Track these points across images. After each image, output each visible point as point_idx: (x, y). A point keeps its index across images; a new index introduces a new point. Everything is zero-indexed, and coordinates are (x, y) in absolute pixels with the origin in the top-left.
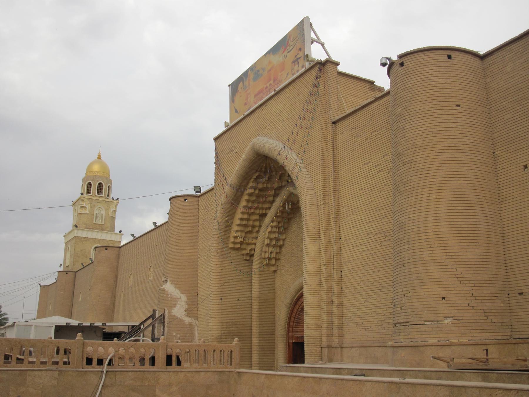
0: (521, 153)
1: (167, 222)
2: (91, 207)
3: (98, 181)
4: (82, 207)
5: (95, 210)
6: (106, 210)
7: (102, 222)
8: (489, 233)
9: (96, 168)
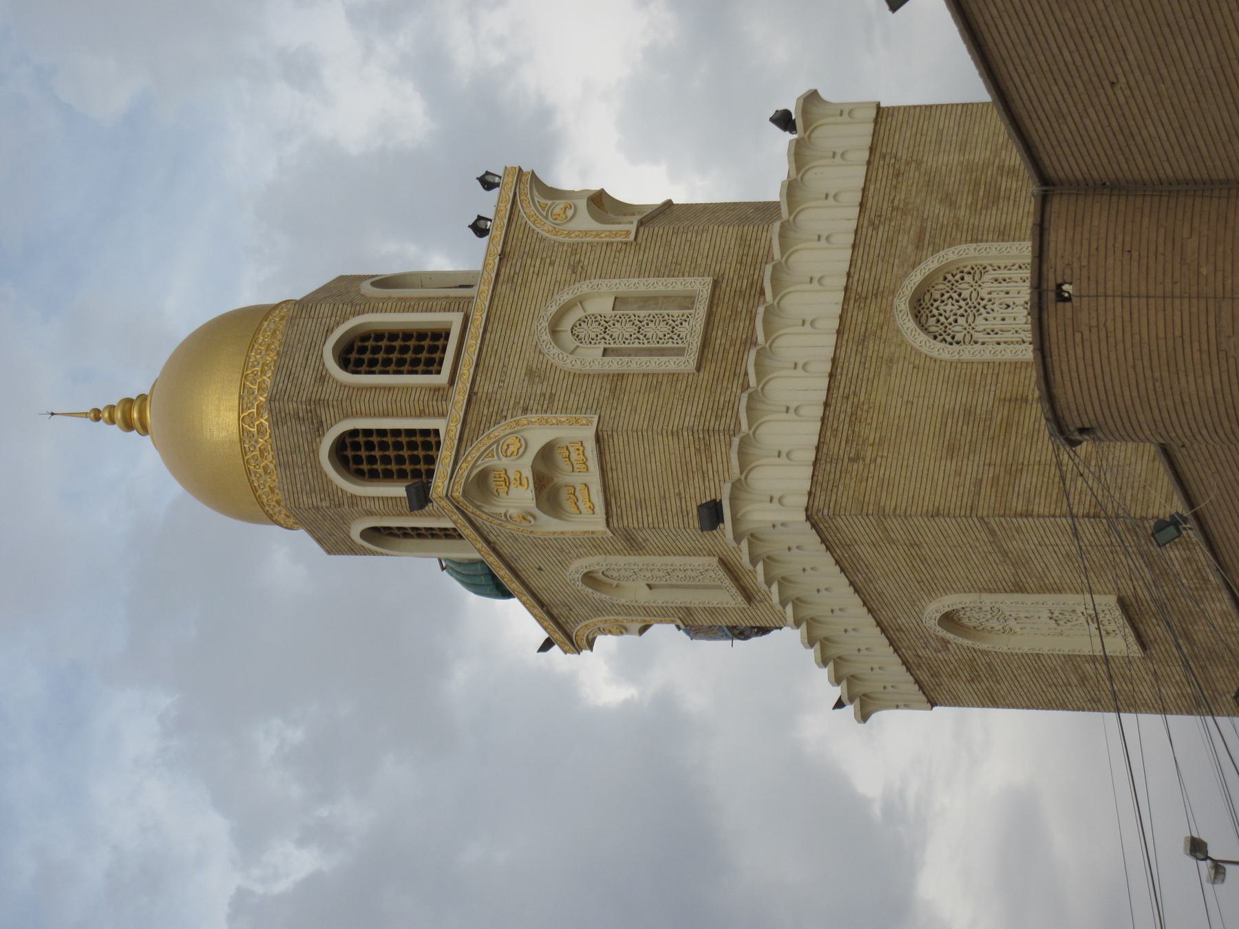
0: (995, 34)
1: (1165, 451)
2: (548, 403)
3: (323, 377)
4: (547, 490)
5: (570, 363)
6: (577, 270)
7: (688, 301)
8: (1078, 82)
9: (221, 416)
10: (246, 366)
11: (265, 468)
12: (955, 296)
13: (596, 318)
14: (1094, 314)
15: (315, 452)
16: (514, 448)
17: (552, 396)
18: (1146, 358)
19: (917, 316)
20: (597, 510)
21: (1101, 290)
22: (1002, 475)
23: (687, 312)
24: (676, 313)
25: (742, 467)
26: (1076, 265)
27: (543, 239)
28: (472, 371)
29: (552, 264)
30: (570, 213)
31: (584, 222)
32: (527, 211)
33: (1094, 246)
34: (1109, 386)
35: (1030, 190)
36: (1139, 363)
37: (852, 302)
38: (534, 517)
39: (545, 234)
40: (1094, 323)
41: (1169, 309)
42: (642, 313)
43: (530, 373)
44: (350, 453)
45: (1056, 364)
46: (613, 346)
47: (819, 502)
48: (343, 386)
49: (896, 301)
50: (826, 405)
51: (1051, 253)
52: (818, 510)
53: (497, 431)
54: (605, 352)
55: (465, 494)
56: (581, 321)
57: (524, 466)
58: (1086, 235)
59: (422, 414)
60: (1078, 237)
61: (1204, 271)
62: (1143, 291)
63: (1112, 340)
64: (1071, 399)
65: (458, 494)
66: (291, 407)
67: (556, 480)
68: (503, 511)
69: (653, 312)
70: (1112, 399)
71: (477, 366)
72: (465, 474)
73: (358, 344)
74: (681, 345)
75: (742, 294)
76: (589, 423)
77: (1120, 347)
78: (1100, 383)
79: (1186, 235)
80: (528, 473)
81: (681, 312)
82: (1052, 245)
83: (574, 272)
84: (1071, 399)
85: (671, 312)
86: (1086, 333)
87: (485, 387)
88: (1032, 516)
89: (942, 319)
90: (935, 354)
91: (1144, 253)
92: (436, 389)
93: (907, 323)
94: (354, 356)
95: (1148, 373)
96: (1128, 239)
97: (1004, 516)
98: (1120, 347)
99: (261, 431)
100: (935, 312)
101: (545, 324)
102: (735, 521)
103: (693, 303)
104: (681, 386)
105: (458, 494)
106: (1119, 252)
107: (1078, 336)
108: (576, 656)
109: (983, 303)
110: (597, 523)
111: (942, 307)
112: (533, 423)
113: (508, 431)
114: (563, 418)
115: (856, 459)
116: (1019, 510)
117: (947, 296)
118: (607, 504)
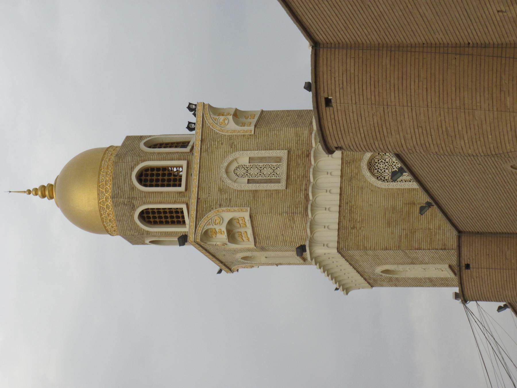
2: (229, 203)
3: (133, 188)
5: (235, 186)
6: (233, 147)
7: (278, 160)
9: (86, 199)
10: (99, 182)
11: (110, 220)
12: (383, 161)
13: (243, 166)
14: (478, 273)
15: (132, 216)
16: (219, 220)
17: (230, 199)
18: (495, 286)
19: (370, 169)
20: (250, 240)
21: (480, 267)
22: (409, 233)
23: (278, 164)
24: (274, 164)
25: (311, 232)
26: (471, 258)
27: (217, 133)
28: (197, 189)
29: (222, 144)
30: (226, 122)
31: (232, 126)
32: (209, 121)
33: (477, 252)
34: (482, 292)
35: (454, 234)
36: (492, 287)
37: (345, 164)
38: (226, 244)
39: (218, 132)
40: (478, 276)
41: (502, 272)
42: (261, 164)
43: (220, 190)
44: (145, 215)
45: (465, 287)
46: (251, 178)
47: (342, 245)
48: (142, 192)
49: (362, 165)
50: (340, 206)
51: (463, 255)
52: (342, 249)
53: (211, 214)
54: (249, 181)
55: (201, 240)
56: (237, 168)
57: (224, 228)
58: (474, 249)
59: (175, 202)
60: (471, 250)
61: (513, 261)
62: (493, 267)
63: (484, 281)
64: (470, 294)
65: (198, 240)
66: (121, 200)
67: (234, 231)
68: (214, 243)
69: (265, 164)
70: (483, 296)
71: (198, 187)
72: (200, 232)
73: (144, 173)
74: (278, 178)
75: (299, 156)
76: (246, 211)
77: (486, 283)
78: (480, 292)
79: (506, 249)
80: (224, 229)
81: (276, 164)
82: (463, 252)
83: (231, 147)
84: (470, 294)
85: (272, 164)
86: (475, 279)
87: (203, 196)
88: (421, 249)
89: (379, 170)
90: (379, 186)
91: (493, 255)
92: (180, 193)
93: (367, 173)
94: (143, 178)
95: (495, 290)
96: (488, 251)
97: (411, 249)
98: (486, 283)
99: (108, 207)
100: (377, 167)
101: (224, 170)
102: (311, 253)
103: (280, 160)
104: (281, 195)
105: (198, 240)
106: (485, 255)
107: (473, 280)
108: (232, 274)
109: (394, 164)
110: (252, 246)
111: (379, 166)
112: (224, 211)
113: (215, 214)
114: (236, 209)
115: (353, 228)
116: (416, 247)
117: (380, 161)
118: (255, 238)
